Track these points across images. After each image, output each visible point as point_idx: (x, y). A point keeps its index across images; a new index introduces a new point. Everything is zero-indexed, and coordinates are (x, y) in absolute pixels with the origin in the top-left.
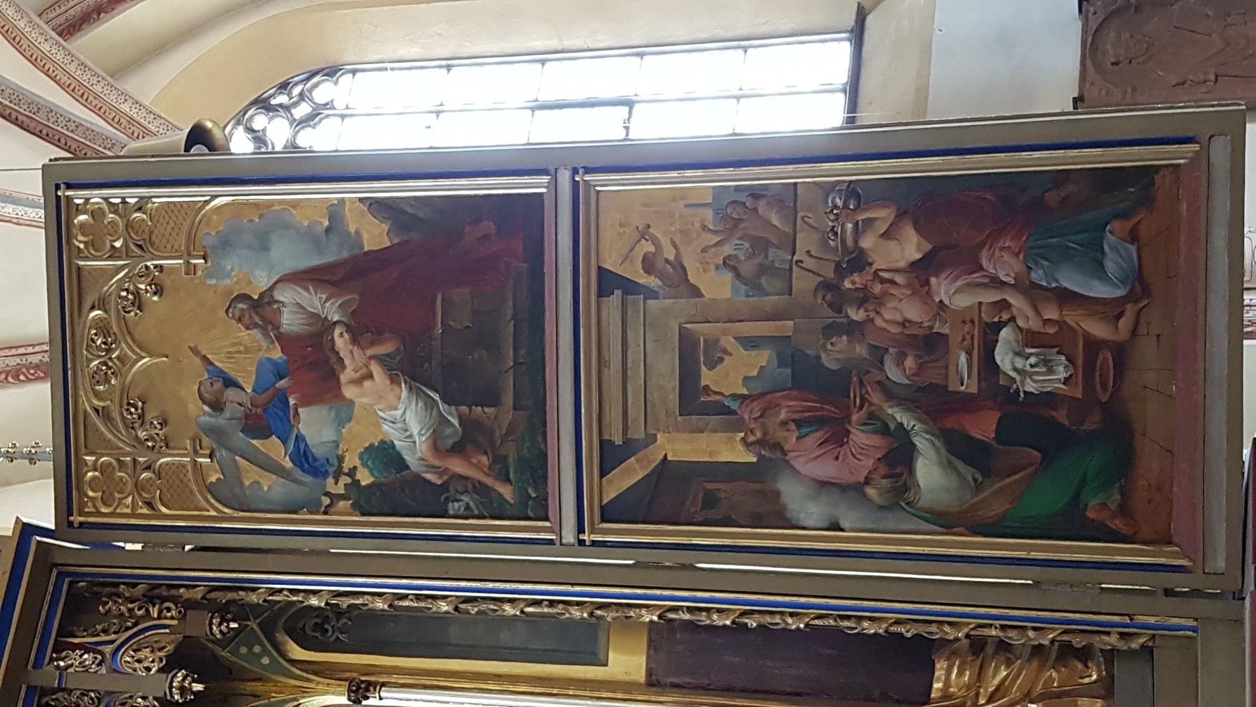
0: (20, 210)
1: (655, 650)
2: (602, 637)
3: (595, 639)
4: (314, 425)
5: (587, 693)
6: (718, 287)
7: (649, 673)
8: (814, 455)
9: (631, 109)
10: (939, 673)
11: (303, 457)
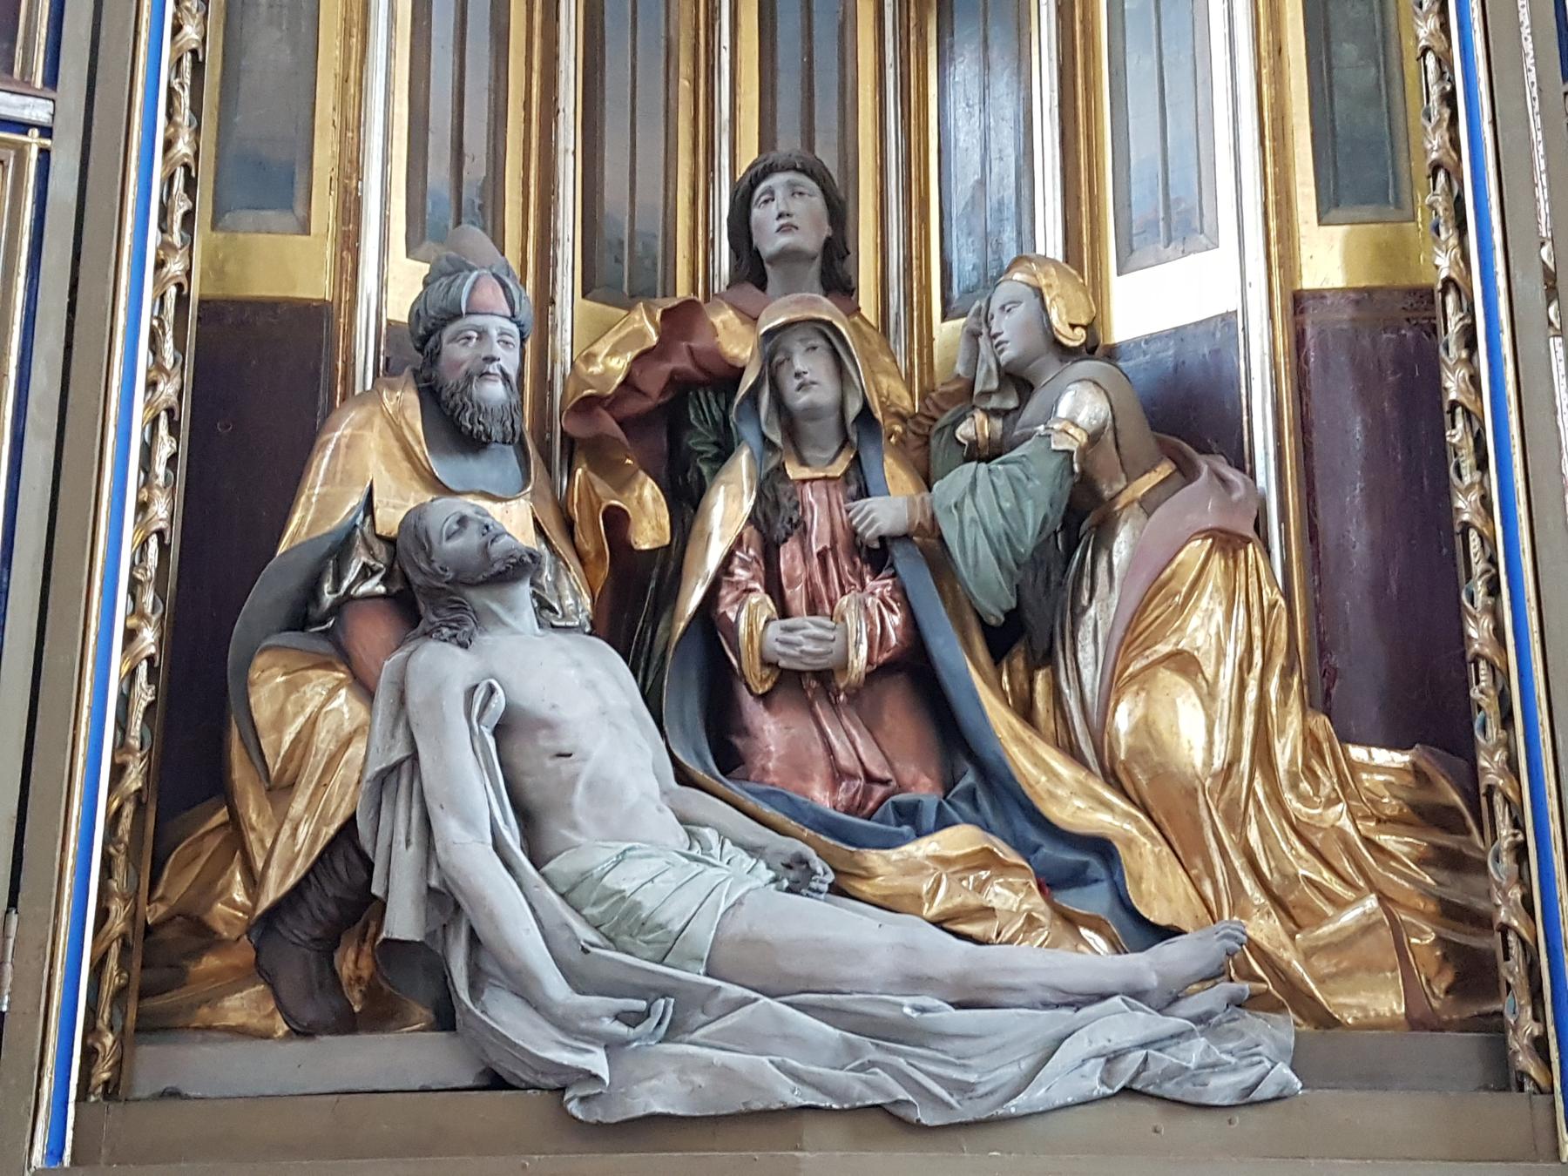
1: (1357, 302)
2: (1367, 212)
3: (1364, 202)
5: (1271, 197)
7: (1319, 295)
8: (858, 798)
9: (573, 888)
10: (1382, 756)
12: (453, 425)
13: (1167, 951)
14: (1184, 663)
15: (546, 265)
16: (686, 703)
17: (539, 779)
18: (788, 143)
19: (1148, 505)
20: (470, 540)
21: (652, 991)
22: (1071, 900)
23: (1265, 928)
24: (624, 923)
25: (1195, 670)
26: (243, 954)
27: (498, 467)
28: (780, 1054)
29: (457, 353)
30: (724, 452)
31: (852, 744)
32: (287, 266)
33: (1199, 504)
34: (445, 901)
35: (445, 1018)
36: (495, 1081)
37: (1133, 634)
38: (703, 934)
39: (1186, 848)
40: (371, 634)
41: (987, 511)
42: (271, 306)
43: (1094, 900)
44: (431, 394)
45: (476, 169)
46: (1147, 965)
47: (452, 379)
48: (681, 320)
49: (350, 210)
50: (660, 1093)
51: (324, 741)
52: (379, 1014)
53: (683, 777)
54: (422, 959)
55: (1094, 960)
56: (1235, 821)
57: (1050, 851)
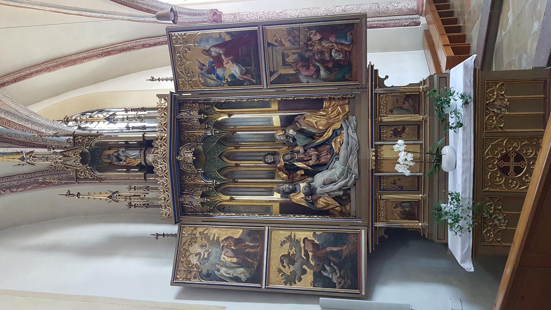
0: (97, 14)
4: (219, 72)
6: (288, 45)
11: (218, 77)
12: (294, 190)
13: (344, 126)
14: (316, 123)
15: (273, 183)
16: (320, 169)
17: (328, 182)
18: (261, 158)
19: (301, 125)
20: (307, 188)
21: (348, 171)
22: (339, 134)
23: (341, 116)
24: (342, 174)
25: (314, 121)
26: (343, 207)
27: (297, 186)
28: (353, 161)
29: (287, 190)
30: (294, 165)
31: (324, 153)
32: (276, 207)
33: (301, 121)
34: (340, 189)
35: (349, 189)
36: (355, 184)
37: (313, 127)
38: (343, 167)
39: (333, 124)
40: (315, 197)
41: (301, 141)
42: (280, 209)
43: (338, 132)
44: (291, 193)
45: (263, 190)
46: (345, 128)
47: (290, 191)
48: (280, 169)
49: (270, 201)
50: (356, 171)
51: (325, 201)
52: (349, 196)
53: (327, 169)
54: (345, 191)
55: (344, 132)
56: (331, 119)
57: (334, 135)
